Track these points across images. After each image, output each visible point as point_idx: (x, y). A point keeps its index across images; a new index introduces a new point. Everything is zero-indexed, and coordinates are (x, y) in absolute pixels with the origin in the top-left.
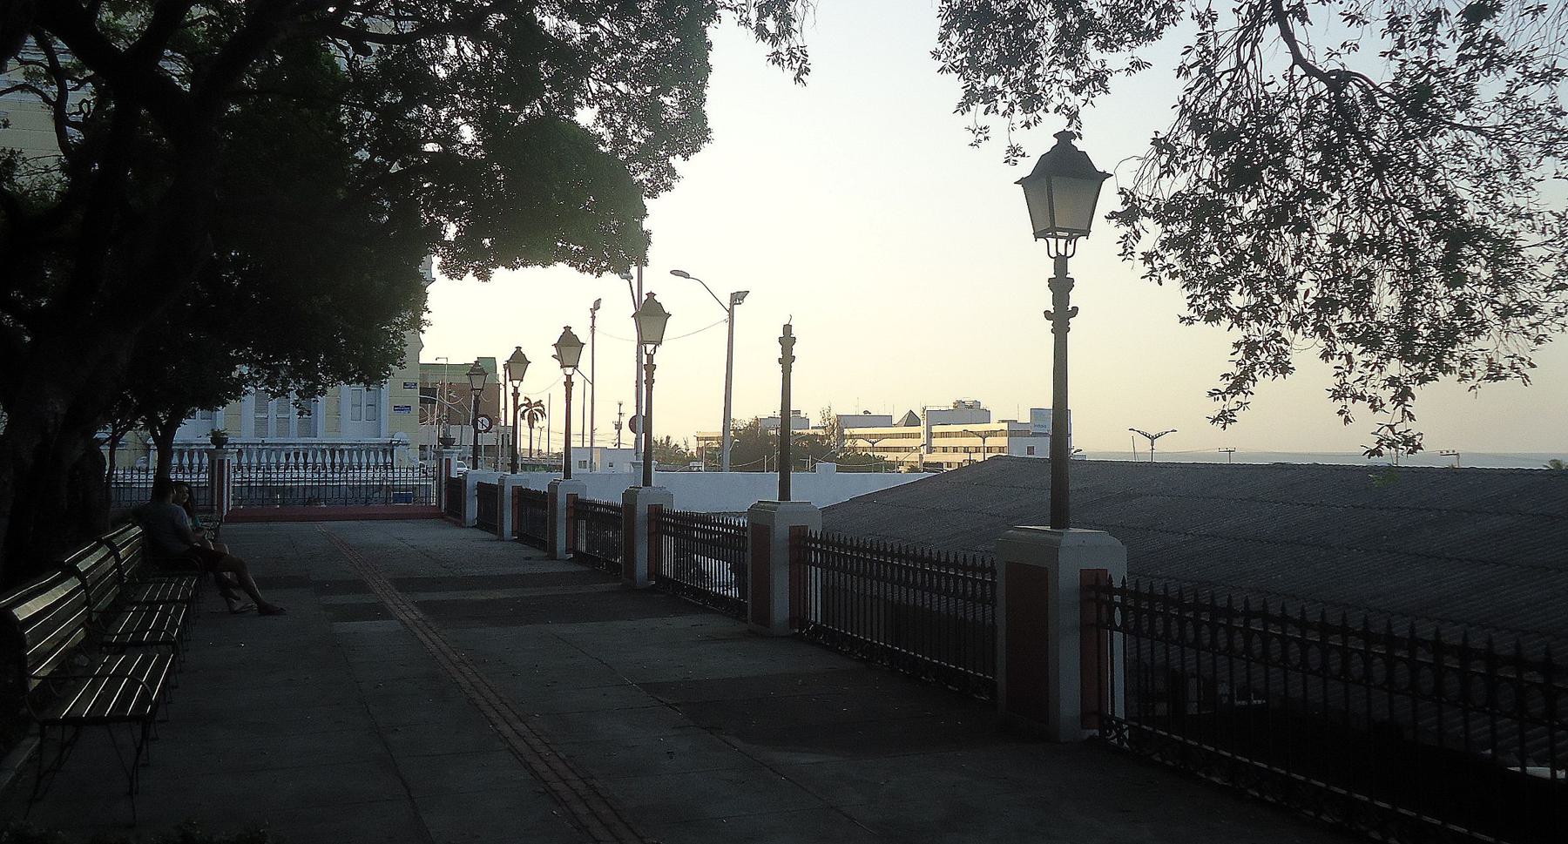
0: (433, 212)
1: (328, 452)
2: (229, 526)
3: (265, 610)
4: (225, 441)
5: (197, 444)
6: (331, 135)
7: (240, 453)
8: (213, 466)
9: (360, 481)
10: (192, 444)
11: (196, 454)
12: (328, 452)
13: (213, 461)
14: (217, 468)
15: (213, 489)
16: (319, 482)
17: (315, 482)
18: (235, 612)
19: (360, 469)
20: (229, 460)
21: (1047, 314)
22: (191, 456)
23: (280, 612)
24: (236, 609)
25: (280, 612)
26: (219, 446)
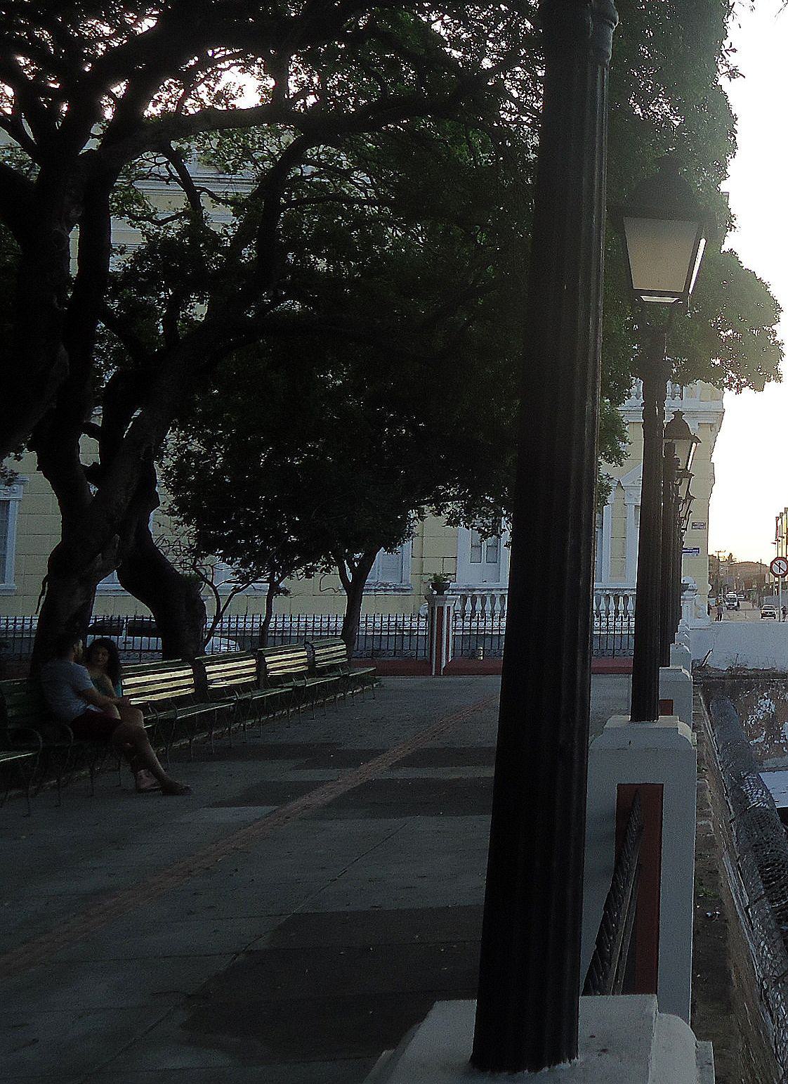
0: (369, 232)
1: (612, 599)
2: (446, 679)
3: (169, 789)
4: (447, 587)
5: (480, 590)
6: (21, 17)
7: (464, 598)
8: (433, 612)
9: (499, 630)
10: (474, 590)
11: (479, 600)
12: (612, 599)
13: (433, 608)
14: (436, 616)
15: (432, 637)
16: (463, 631)
17: (392, 631)
18: (140, 791)
19: (463, 618)
20: (449, 607)
21: (779, 378)
22: (474, 603)
23: (184, 791)
24: (143, 786)
25: (184, 791)
26: (440, 593)
